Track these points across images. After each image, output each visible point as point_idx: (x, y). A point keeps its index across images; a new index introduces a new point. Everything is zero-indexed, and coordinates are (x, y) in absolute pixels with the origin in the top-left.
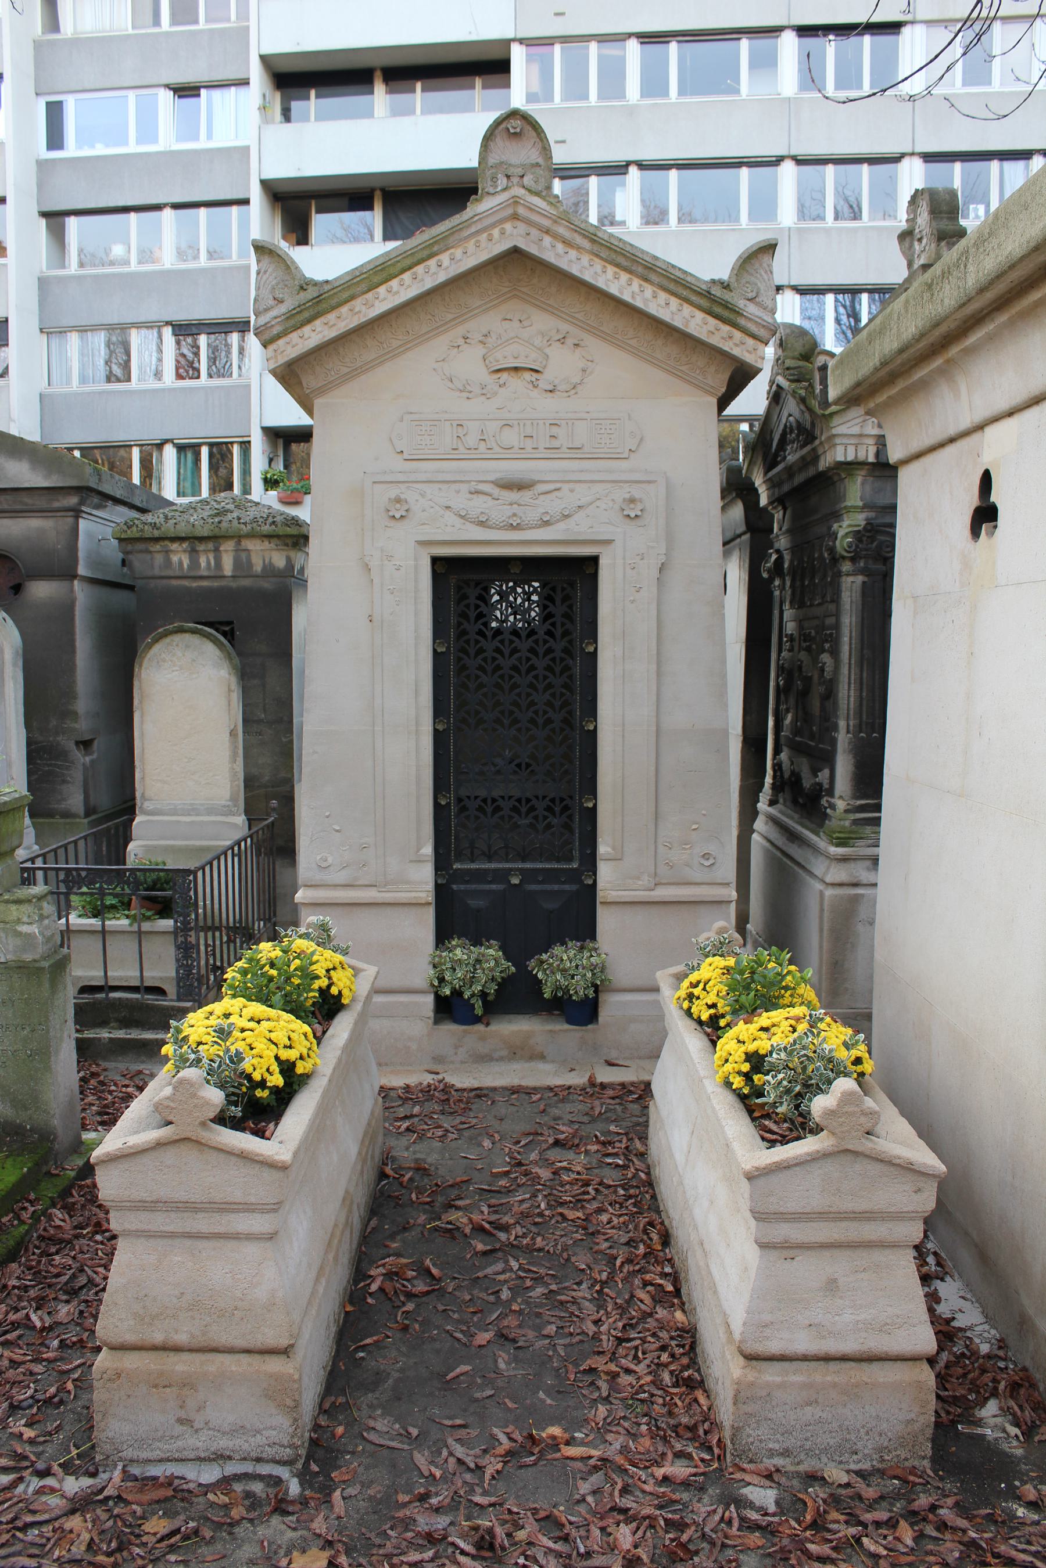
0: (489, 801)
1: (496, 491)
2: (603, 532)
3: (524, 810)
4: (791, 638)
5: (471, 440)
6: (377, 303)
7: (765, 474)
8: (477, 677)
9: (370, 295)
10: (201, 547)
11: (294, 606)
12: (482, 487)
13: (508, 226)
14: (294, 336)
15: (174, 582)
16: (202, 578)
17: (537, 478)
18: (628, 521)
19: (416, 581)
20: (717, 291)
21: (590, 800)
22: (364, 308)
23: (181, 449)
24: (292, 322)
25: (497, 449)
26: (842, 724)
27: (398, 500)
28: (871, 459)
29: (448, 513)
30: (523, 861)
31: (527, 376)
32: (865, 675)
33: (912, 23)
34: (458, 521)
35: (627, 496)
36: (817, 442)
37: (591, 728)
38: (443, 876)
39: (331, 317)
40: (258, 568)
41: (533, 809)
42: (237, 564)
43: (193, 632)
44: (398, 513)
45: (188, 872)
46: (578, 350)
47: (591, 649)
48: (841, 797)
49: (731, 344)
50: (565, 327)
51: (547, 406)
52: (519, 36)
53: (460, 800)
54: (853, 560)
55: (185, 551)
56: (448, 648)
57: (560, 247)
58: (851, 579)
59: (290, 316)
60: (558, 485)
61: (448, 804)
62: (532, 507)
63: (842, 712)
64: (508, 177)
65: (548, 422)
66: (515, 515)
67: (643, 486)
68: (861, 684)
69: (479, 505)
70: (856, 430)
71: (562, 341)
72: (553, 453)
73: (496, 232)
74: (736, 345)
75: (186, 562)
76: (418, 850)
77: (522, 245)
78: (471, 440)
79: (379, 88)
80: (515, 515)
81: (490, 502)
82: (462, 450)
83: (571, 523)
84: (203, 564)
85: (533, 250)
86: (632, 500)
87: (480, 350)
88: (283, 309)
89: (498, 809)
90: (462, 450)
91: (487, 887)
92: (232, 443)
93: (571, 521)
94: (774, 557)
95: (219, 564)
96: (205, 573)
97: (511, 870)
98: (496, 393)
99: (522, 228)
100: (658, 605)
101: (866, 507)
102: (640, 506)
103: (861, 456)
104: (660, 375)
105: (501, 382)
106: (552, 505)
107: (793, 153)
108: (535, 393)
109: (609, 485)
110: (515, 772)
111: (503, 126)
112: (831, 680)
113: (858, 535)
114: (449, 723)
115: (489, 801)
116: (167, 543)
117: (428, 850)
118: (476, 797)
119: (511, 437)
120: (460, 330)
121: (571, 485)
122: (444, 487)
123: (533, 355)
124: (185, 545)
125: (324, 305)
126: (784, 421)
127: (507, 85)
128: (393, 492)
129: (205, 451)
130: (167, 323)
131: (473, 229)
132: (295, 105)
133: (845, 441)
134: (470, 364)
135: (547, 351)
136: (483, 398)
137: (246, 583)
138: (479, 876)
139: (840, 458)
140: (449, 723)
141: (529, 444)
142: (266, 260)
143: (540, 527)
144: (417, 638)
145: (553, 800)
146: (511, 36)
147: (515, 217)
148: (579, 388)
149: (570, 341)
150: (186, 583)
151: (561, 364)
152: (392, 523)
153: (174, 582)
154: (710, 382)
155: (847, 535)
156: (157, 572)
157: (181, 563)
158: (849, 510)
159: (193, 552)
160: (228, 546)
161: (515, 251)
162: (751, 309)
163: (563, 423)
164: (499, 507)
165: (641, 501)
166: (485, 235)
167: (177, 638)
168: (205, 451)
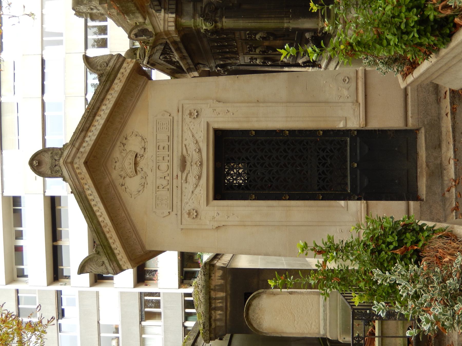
0: (320, 176)
1: (186, 172)
2: (203, 126)
3: (324, 161)
4: (252, 59)
5: (165, 182)
6: (105, 222)
7: (186, 73)
8: (266, 181)
9: (102, 224)
10: (213, 306)
11: (238, 267)
12: (184, 178)
13: (76, 166)
14: (119, 257)
15: (228, 317)
16: (226, 306)
17: (180, 154)
18: (199, 116)
19: (224, 206)
20: (104, 78)
21: (319, 133)
22: (107, 227)
23: (186, 319)
24: (112, 258)
25: (168, 172)
26: (286, 25)
27: (189, 214)
28: (174, 15)
29: (195, 192)
30: (347, 162)
31: (138, 159)
32: (265, 16)
33: (42, 55)
34: (198, 188)
35: (188, 116)
36: (168, 41)
37: (288, 132)
38: (354, 197)
39: (111, 241)
40: (222, 282)
41: (323, 157)
42: (221, 291)
43: (248, 309)
44: (195, 214)
45: (353, 312)
46: (128, 138)
47: (254, 133)
48: (318, 24)
49: (125, 73)
50: (118, 143)
51: (151, 151)
52: (43, 193)
53: (319, 189)
54: (216, 22)
55: (215, 313)
56: (253, 194)
57: (85, 144)
58: (224, 24)
59: (110, 260)
60: (184, 145)
61: (322, 194)
62: (193, 156)
63: (280, 25)
64: (55, 166)
65: (158, 150)
66: (196, 164)
67: (184, 109)
68: (268, 17)
69: (192, 180)
70: (162, 22)
71: (124, 145)
72: (170, 148)
73: (78, 171)
74: (126, 71)
75: (219, 312)
76: (342, 207)
77: (83, 160)
78: (165, 182)
79: (60, 243)
80: (196, 164)
81: (190, 174)
82: (168, 187)
83: (200, 140)
84: (221, 305)
85: (85, 155)
86: (190, 114)
87: (127, 179)
88: (106, 262)
89: (323, 172)
90: (168, 187)
91: (358, 177)
92: (184, 300)
93: (199, 140)
94: (219, 69)
95: (221, 298)
96: (225, 304)
97: (350, 167)
98: (145, 172)
99: (76, 160)
100: (235, 103)
101: (194, 17)
102: (193, 111)
103: (173, 20)
104: (139, 103)
105: (140, 170)
106: (192, 147)
107: (84, 95)
108: (146, 156)
109: (184, 124)
110: (307, 165)
111: (35, 168)
112: (267, 33)
113: (206, 20)
114: (285, 194)
115: (320, 176)
116: (212, 320)
117: (342, 203)
118: (318, 182)
119: (164, 166)
120: (119, 188)
121: (184, 140)
122: (183, 194)
123: (129, 156)
124: (213, 312)
125: (106, 244)
126: (163, 62)
127: (60, 197)
128: (186, 216)
129: (188, 310)
130: (140, 323)
131: (76, 181)
132: (65, 274)
133: (166, 26)
134: (133, 184)
135: (128, 151)
136: (147, 177)
137: (228, 287)
138: (353, 181)
139: (173, 28)
140: (285, 194)
141: (167, 158)
142: (87, 268)
143: (201, 153)
144: (248, 206)
145: (320, 163)
146: (43, 195)
147: (72, 163)
148: (144, 138)
149: (124, 141)
150: (228, 312)
151: (134, 145)
152: (199, 216)
153: (228, 317)
154: (141, 83)
155: (206, 26)
156: (223, 324)
157: (220, 314)
158: (195, 26)
159: (216, 309)
160: (213, 294)
161: (86, 163)
162: (111, 64)
163: (158, 144)
164: (193, 170)
165: (190, 111)
166: (79, 176)
167: (251, 316)
168: (188, 310)
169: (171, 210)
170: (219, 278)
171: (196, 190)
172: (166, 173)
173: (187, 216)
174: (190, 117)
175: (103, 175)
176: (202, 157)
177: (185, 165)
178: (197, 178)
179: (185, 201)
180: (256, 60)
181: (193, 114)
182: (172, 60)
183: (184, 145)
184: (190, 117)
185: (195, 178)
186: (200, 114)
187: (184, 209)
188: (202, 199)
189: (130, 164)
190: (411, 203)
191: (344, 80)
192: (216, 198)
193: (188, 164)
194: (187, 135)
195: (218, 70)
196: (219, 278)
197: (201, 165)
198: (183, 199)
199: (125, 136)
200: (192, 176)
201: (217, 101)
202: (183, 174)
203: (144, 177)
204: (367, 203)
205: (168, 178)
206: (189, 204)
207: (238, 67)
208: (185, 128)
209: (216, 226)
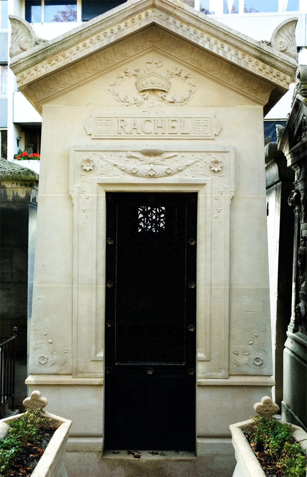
7: (290, 149)
12: (134, 154)
19: (97, 205)
20: (265, 47)
21: (192, 327)
27: (88, 161)
29: (115, 168)
31: (159, 94)
35: (213, 160)
40: (10, 198)
44: (88, 169)
47: (193, 243)
50: (180, 67)
51: (169, 111)
56: (114, 242)
60: (176, 154)
66: (152, 170)
71: (178, 75)
73: (143, 15)
76: (96, 354)
78: (128, 129)
80: (152, 170)
85: (163, 24)
87: (133, 80)
94: (295, 194)
99: (158, 12)
104: (232, 93)
105: (145, 97)
106: (173, 165)
109: (204, 154)
117: (101, 354)
119: (149, 127)
121: (183, 154)
126: (301, 119)
128: (86, 156)
134: (127, 87)
135: (170, 80)
140: (114, 284)
141: (160, 131)
143: (166, 176)
144: (97, 236)
151: (178, 88)
152: (84, 173)
161: (153, 25)
164: (144, 166)
165: (221, 162)
169: (93, 137)
170: (15, 194)
171: (119, 170)
172: (140, 131)
173: (85, 159)
174: (212, 162)
175: (139, 48)
176: (160, 177)
177: (150, 156)
178: (133, 172)
179: (104, 155)
180: (304, 246)
181: (216, 165)
182: (303, 132)
183: (176, 154)
184: (212, 162)
185: (134, 168)
186: (217, 174)
187: (93, 154)
188: (107, 178)
189: (153, 84)
190: (101, 440)
191: (257, 359)
192: (110, 196)
193: (152, 159)
194: (189, 159)
195: (293, 193)
196: (15, 194)
197: (150, 176)
198: (106, 153)
199: (189, 76)
200: (136, 164)
201: (233, 197)
202: (139, 153)
203: (136, 102)
204: (99, 386)
205: (134, 132)
206: (101, 161)
207: (296, 221)
208: (198, 155)
209: (73, 195)
